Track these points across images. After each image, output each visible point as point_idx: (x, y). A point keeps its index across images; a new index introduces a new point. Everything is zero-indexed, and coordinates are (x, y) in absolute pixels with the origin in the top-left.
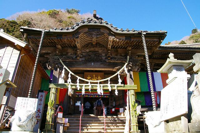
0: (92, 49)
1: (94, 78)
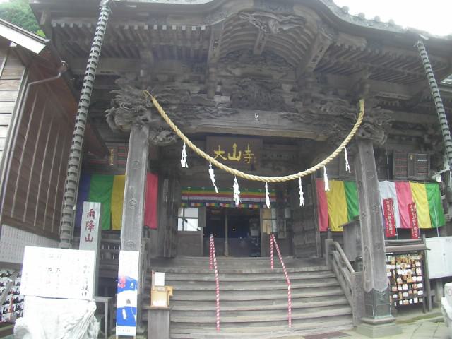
0: (251, 69)
1: (234, 154)
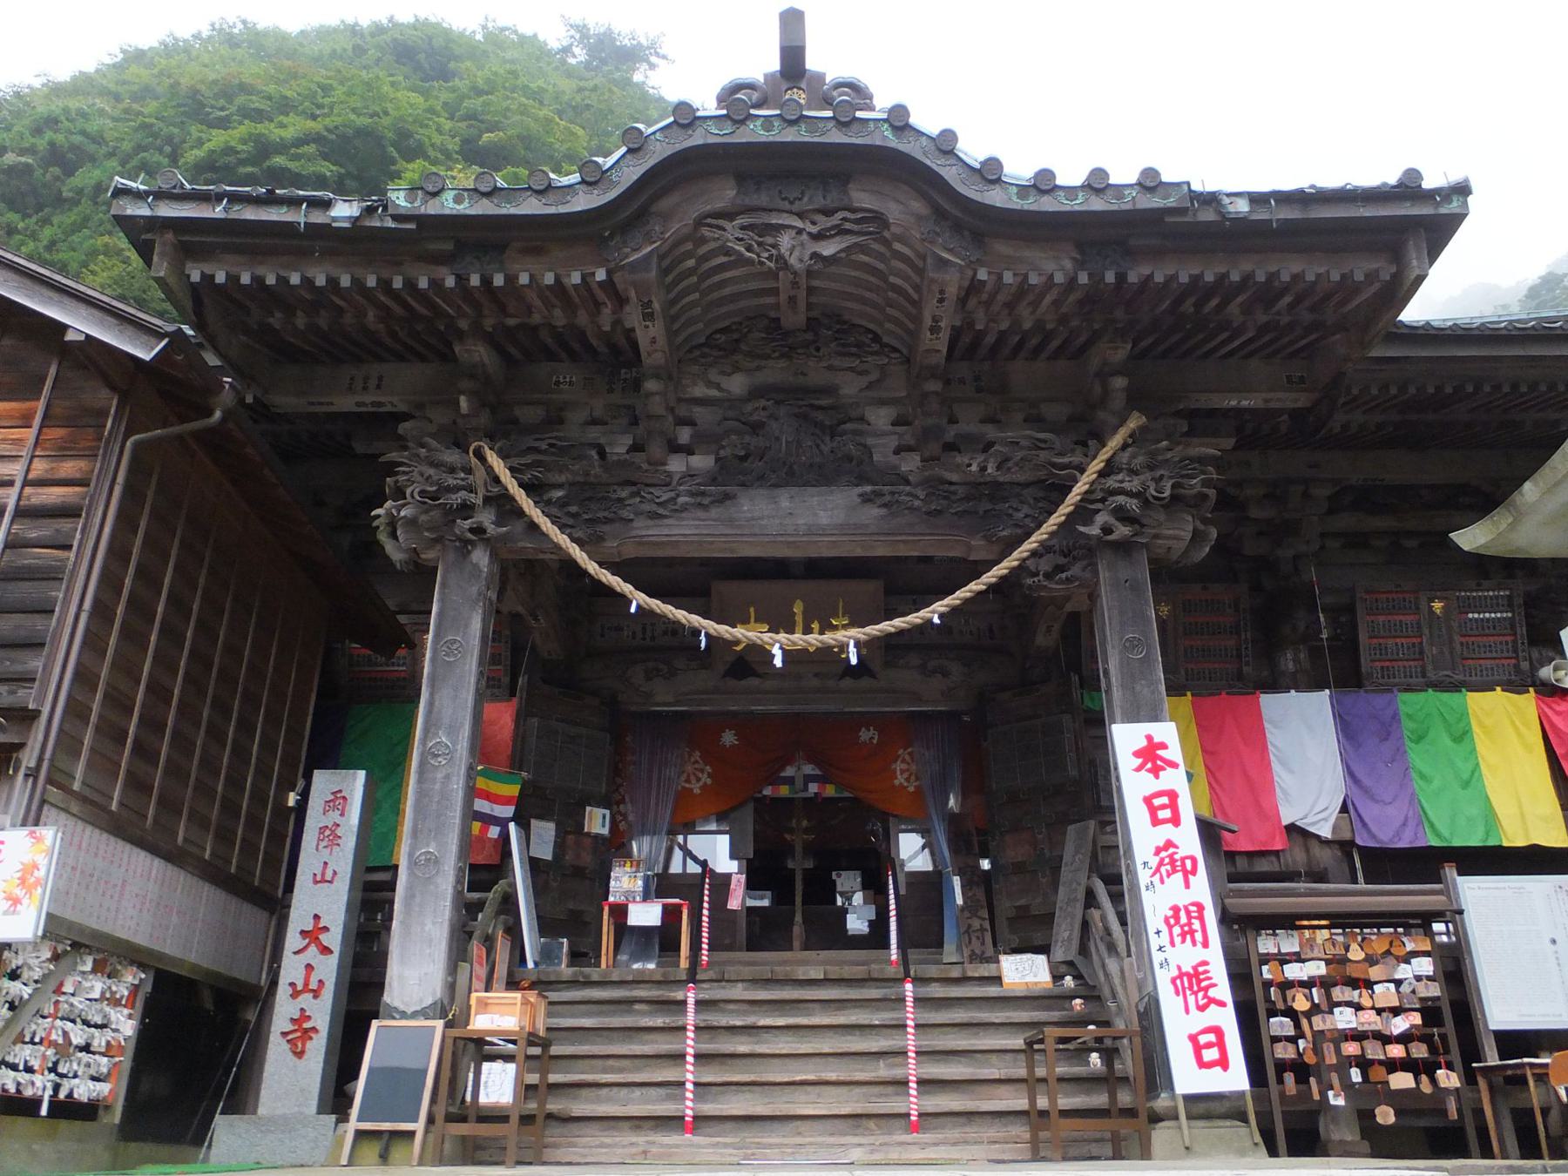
0: (775, 372)
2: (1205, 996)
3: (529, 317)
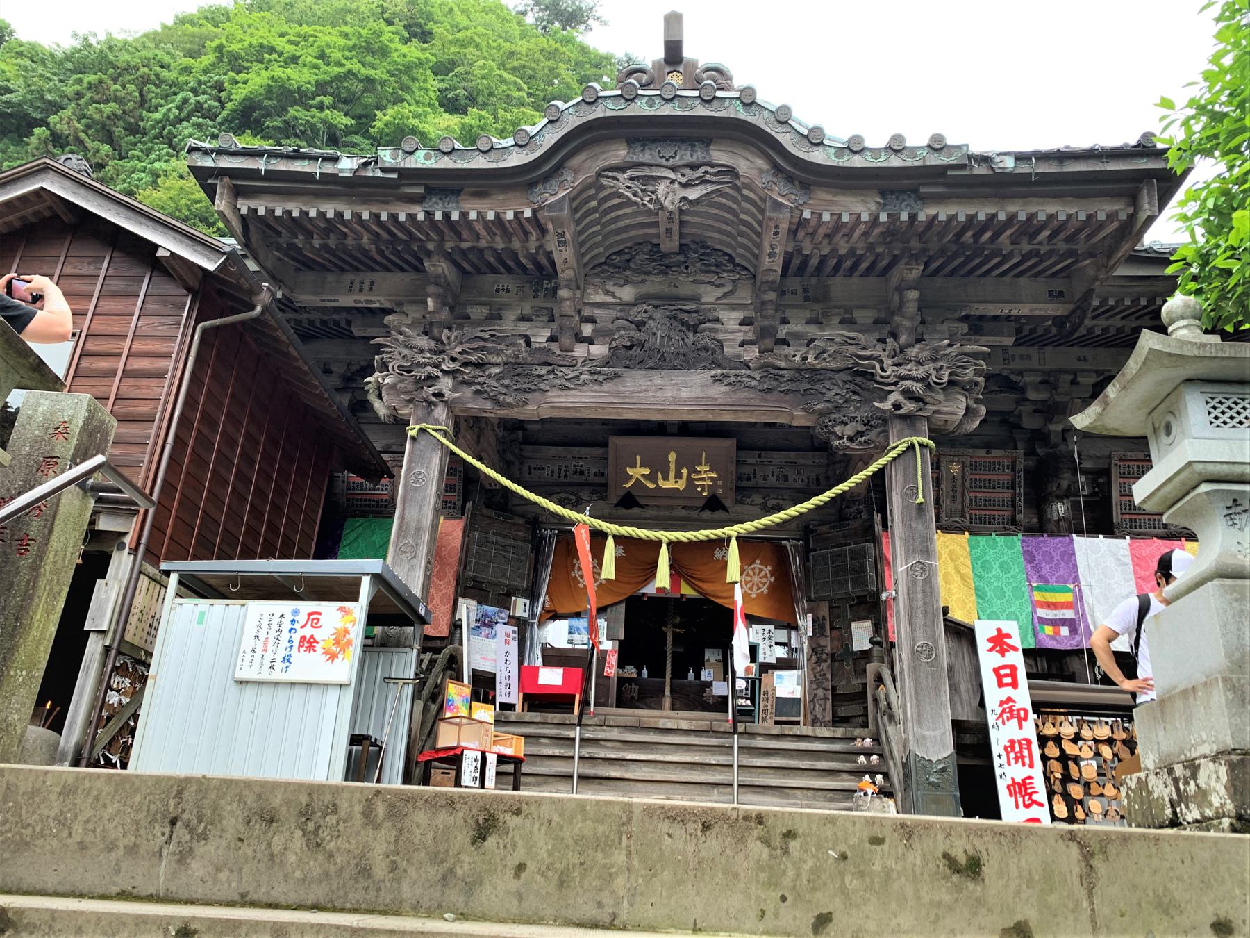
1: (672, 474)
2: (1030, 799)
3: (477, 241)
